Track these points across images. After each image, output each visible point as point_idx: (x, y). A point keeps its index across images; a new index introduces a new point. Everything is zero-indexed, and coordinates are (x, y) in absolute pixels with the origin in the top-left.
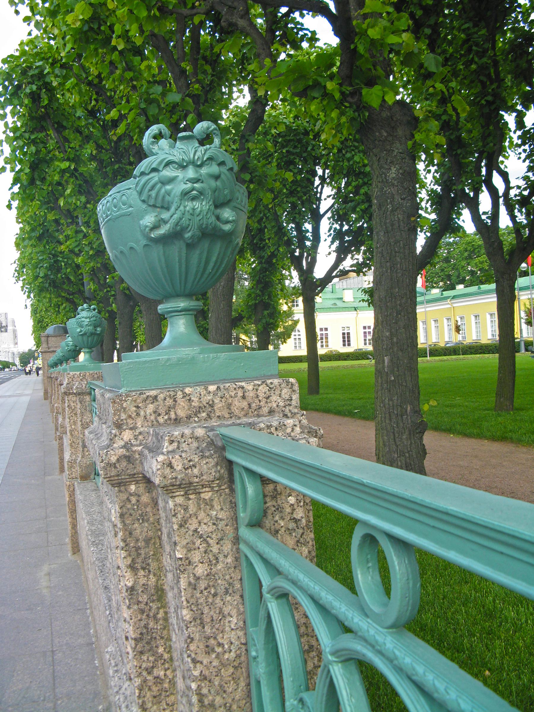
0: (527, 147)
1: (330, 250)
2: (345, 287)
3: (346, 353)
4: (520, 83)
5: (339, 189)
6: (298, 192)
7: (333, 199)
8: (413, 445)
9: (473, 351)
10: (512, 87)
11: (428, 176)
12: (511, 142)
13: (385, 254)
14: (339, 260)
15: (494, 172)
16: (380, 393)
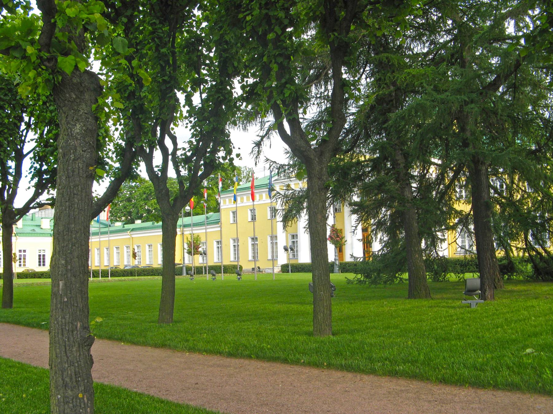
0: (192, 119)
1: (30, 185)
2: (43, 216)
3: (41, 272)
4: (191, 71)
5: (42, 134)
6: (5, 133)
7: (36, 142)
8: (82, 356)
9: (146, 273)
10: (185, 73)
11: (116, 131)
12: (181, 114)
13: (65, 194)
14: (37, 194)
15: (166, 135)
16: (54, 311)
